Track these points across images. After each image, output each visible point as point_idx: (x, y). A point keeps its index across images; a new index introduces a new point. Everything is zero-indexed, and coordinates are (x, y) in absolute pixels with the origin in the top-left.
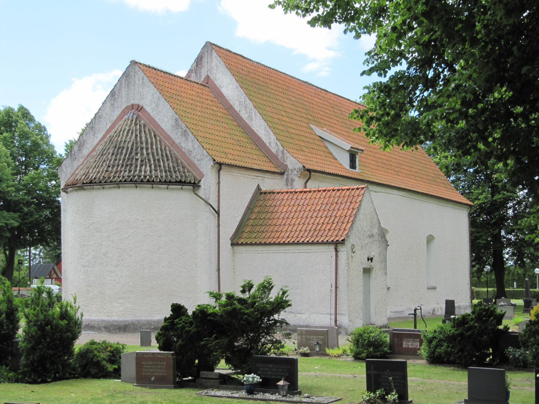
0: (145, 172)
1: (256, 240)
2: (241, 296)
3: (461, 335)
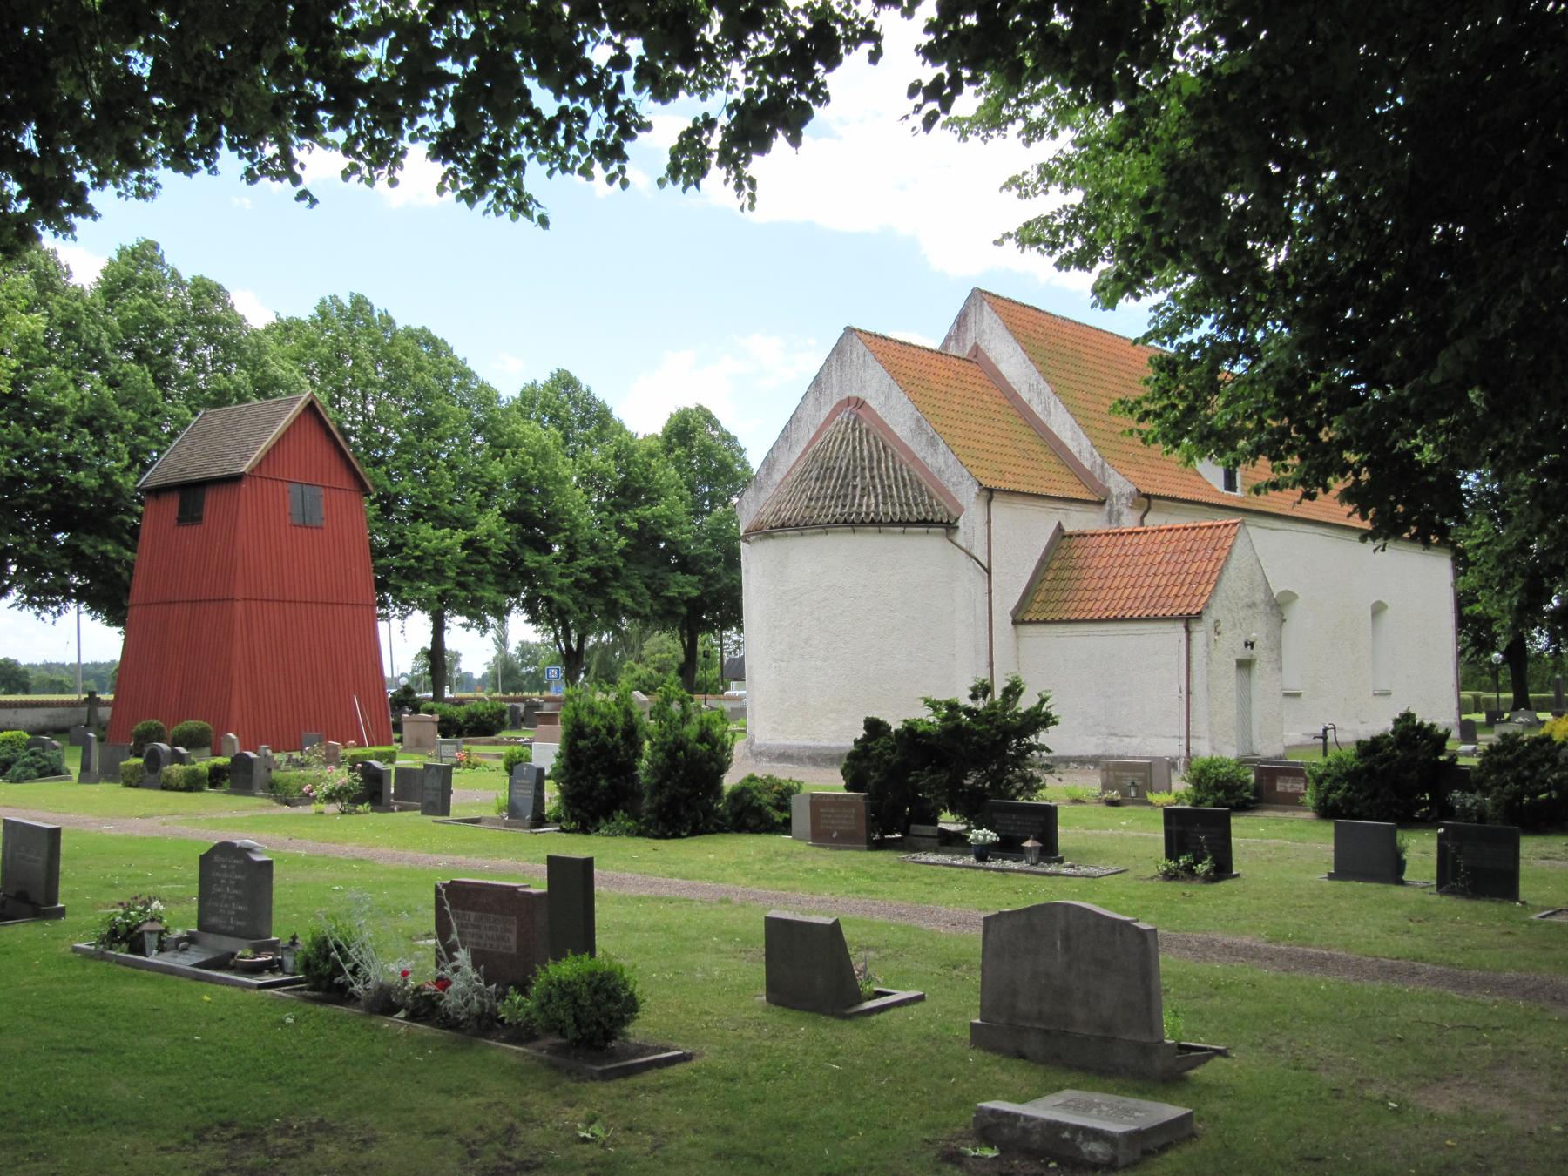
0: (868, 506)
1: (1053, 616)
2: (971, 704)
3: (1370, 770)
